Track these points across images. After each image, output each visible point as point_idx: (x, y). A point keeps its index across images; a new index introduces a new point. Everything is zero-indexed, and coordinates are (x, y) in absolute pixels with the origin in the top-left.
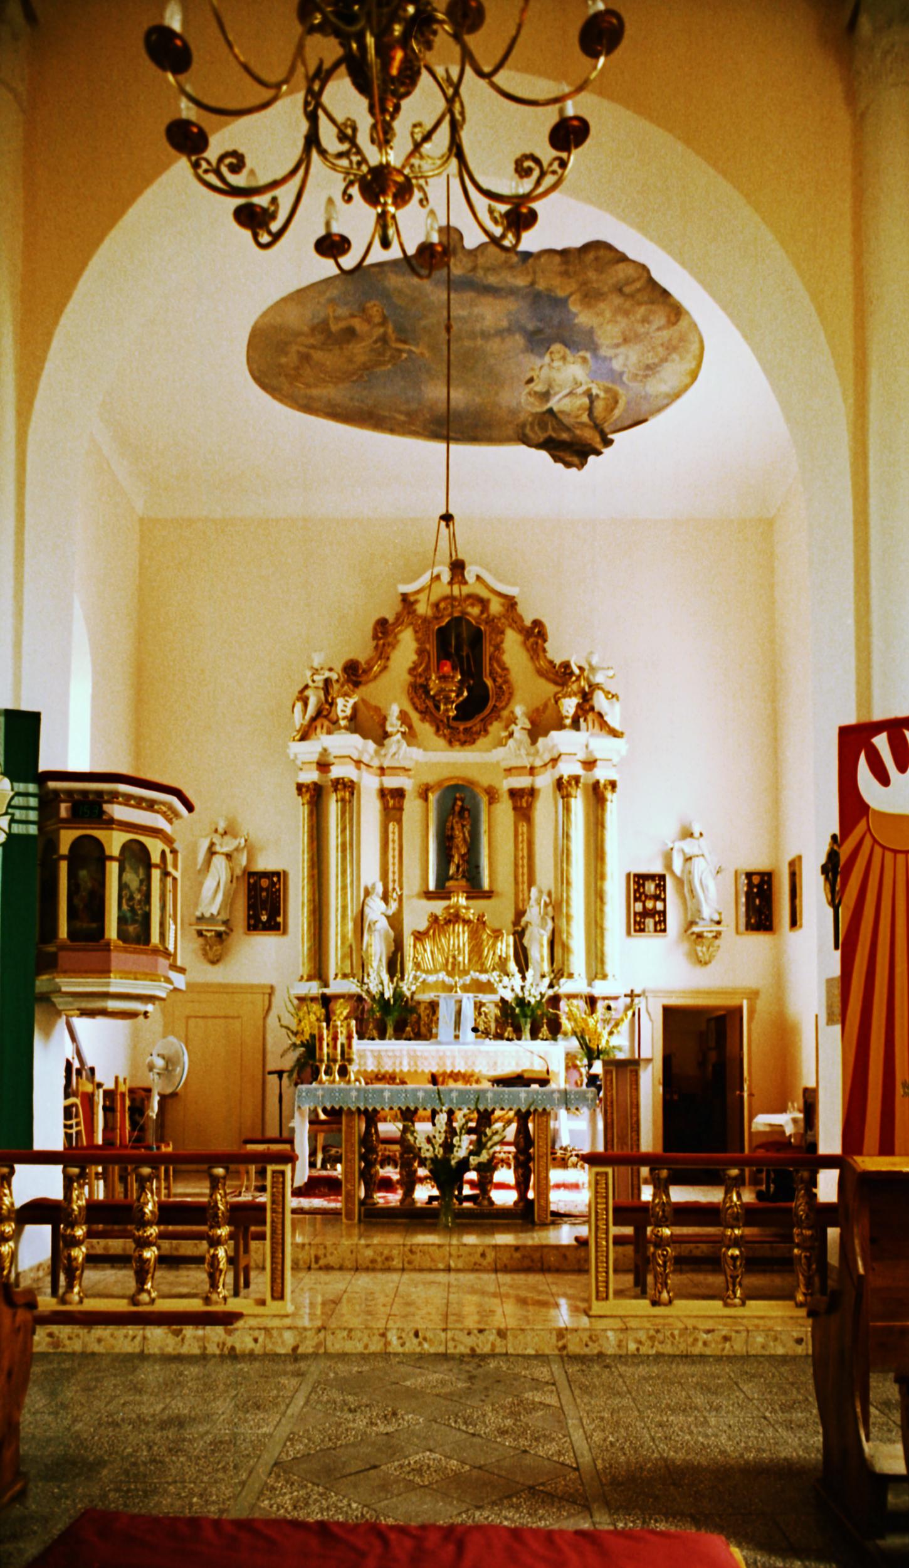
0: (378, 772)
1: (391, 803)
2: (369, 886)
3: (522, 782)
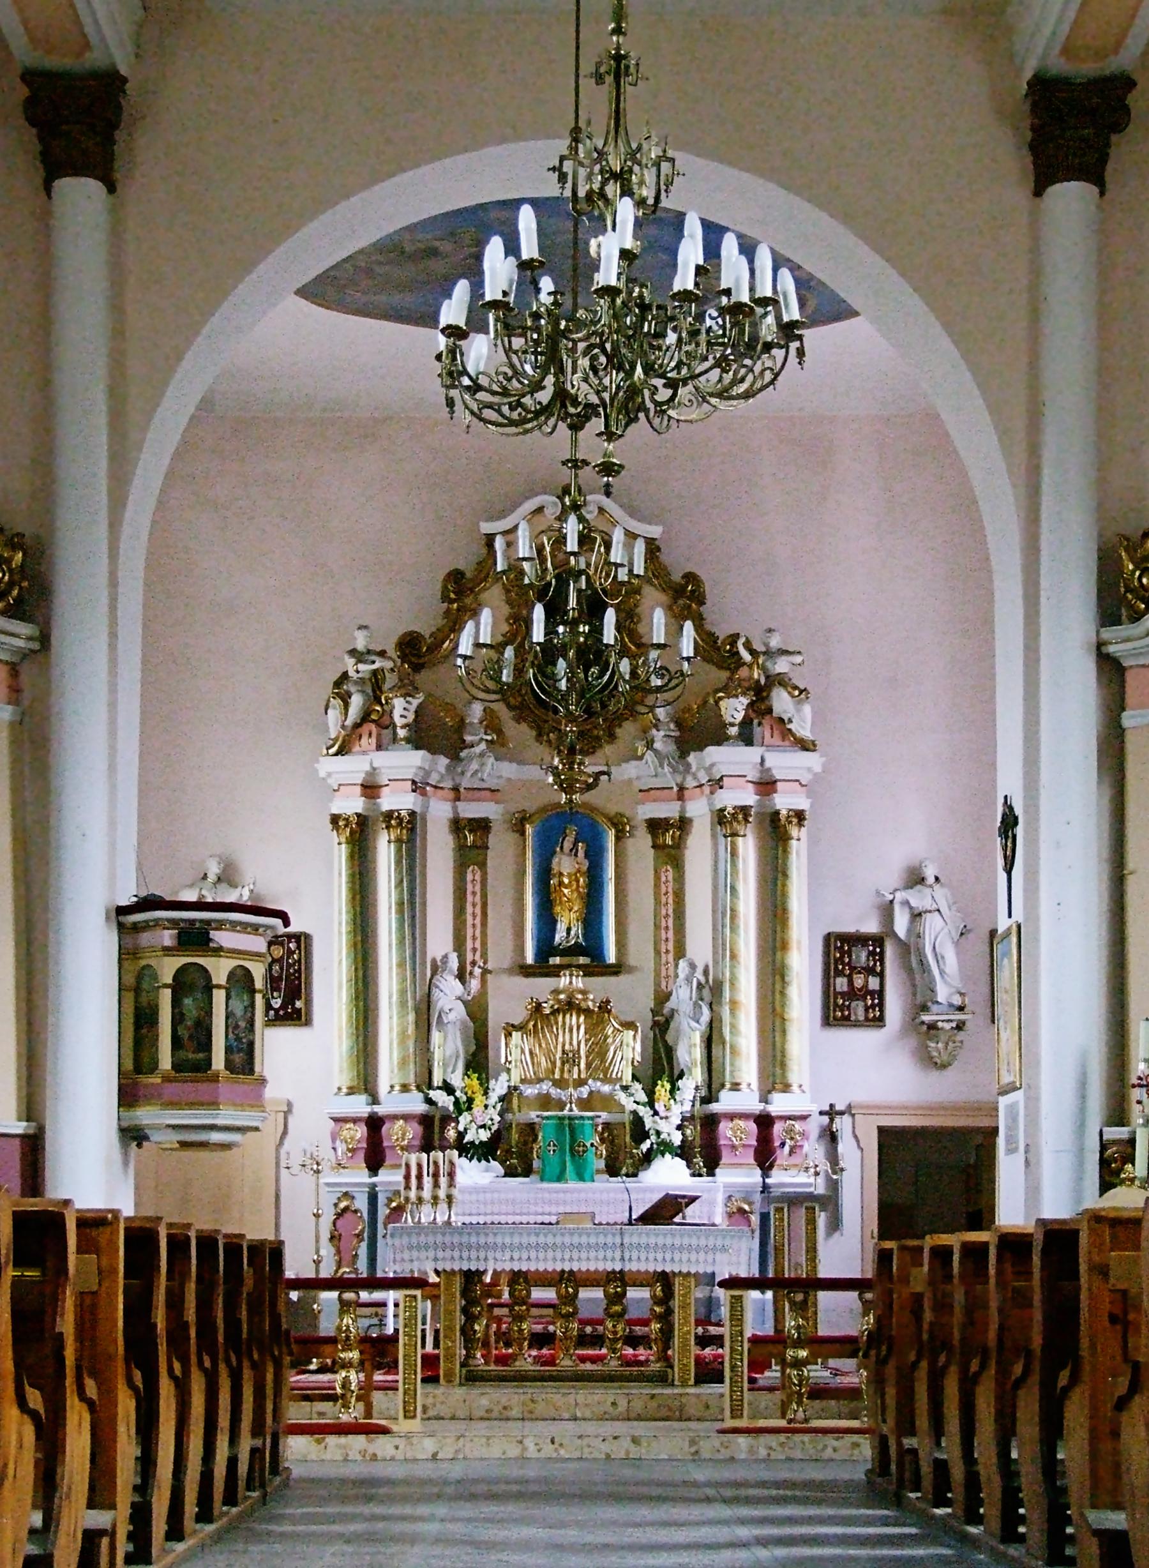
0: (451, 795)
1: (470, 838)
3: (667, 810)
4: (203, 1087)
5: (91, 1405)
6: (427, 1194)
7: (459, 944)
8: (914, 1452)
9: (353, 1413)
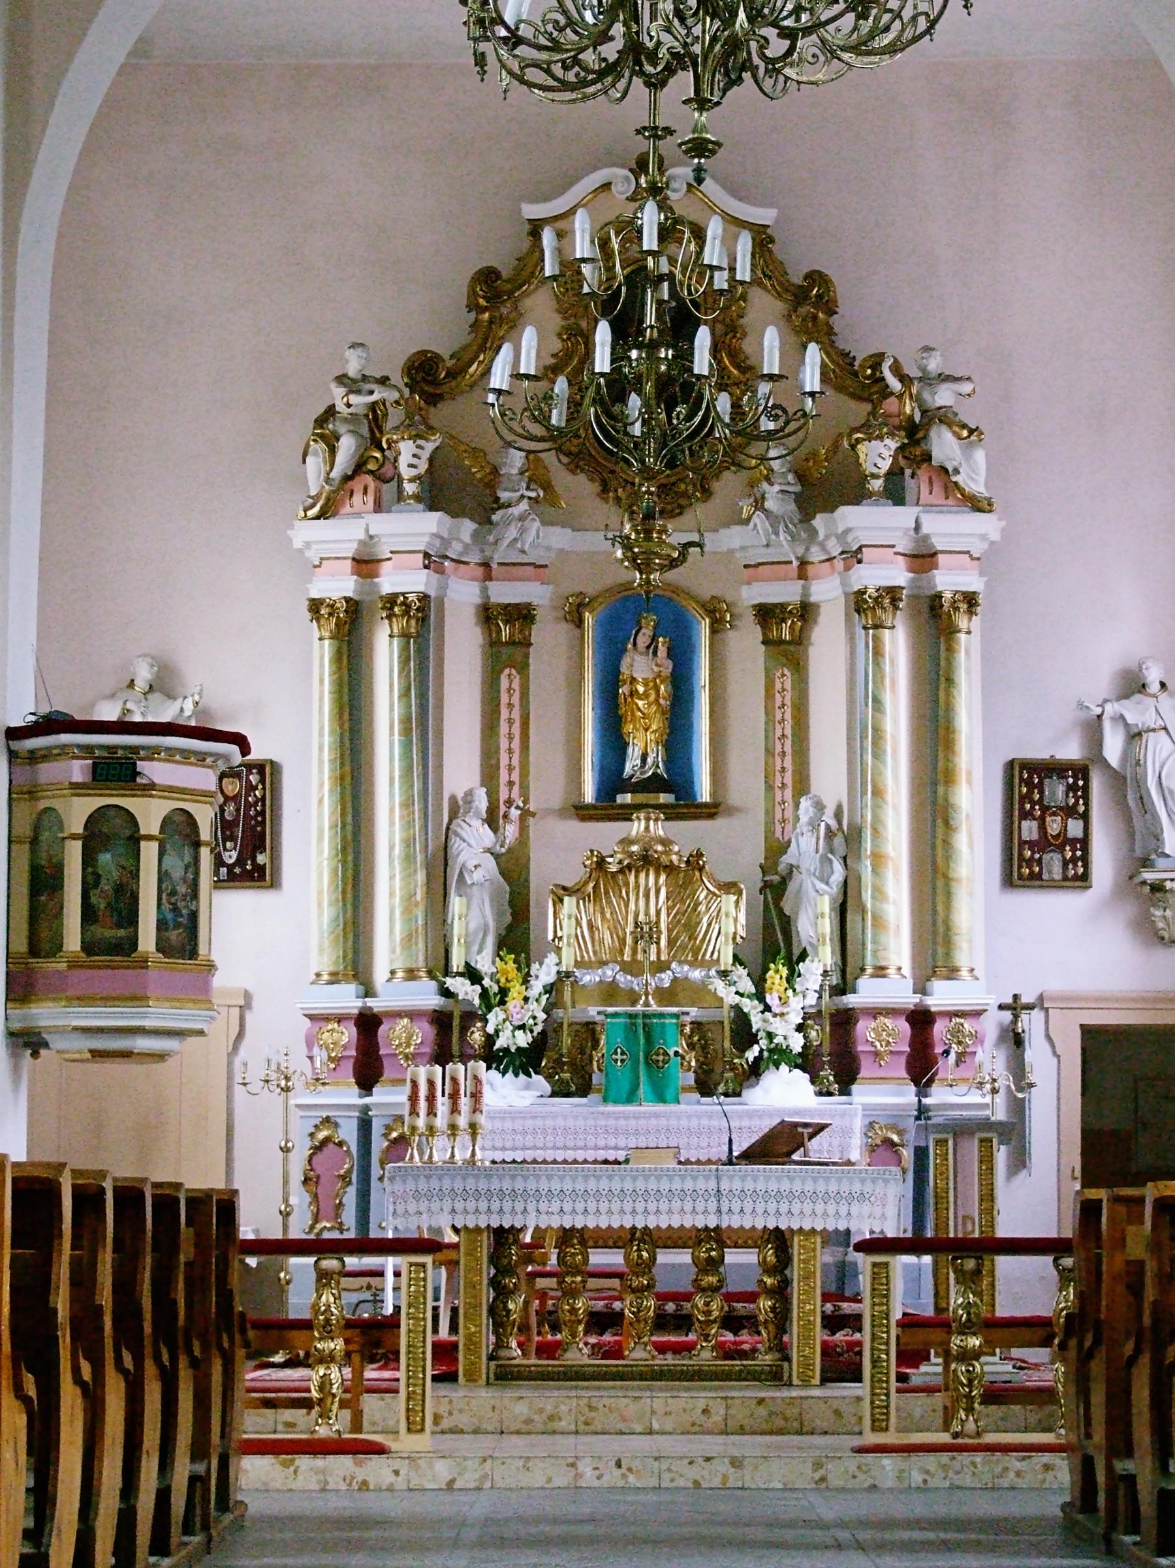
0: (480, 571)
2: (460, 796)
3: (785, 592)
7: (489, 777)
9: (336, 1425)
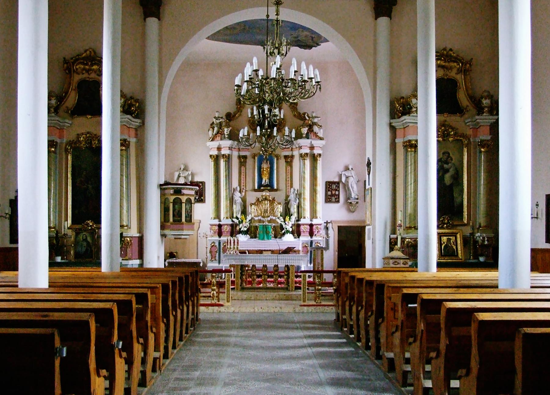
1: (242, 160)
4: (181, 226)
5: (154, 333)
6: (232, 247)
7: (240, 185)
8: (345, 319)
9: (215, 301)
